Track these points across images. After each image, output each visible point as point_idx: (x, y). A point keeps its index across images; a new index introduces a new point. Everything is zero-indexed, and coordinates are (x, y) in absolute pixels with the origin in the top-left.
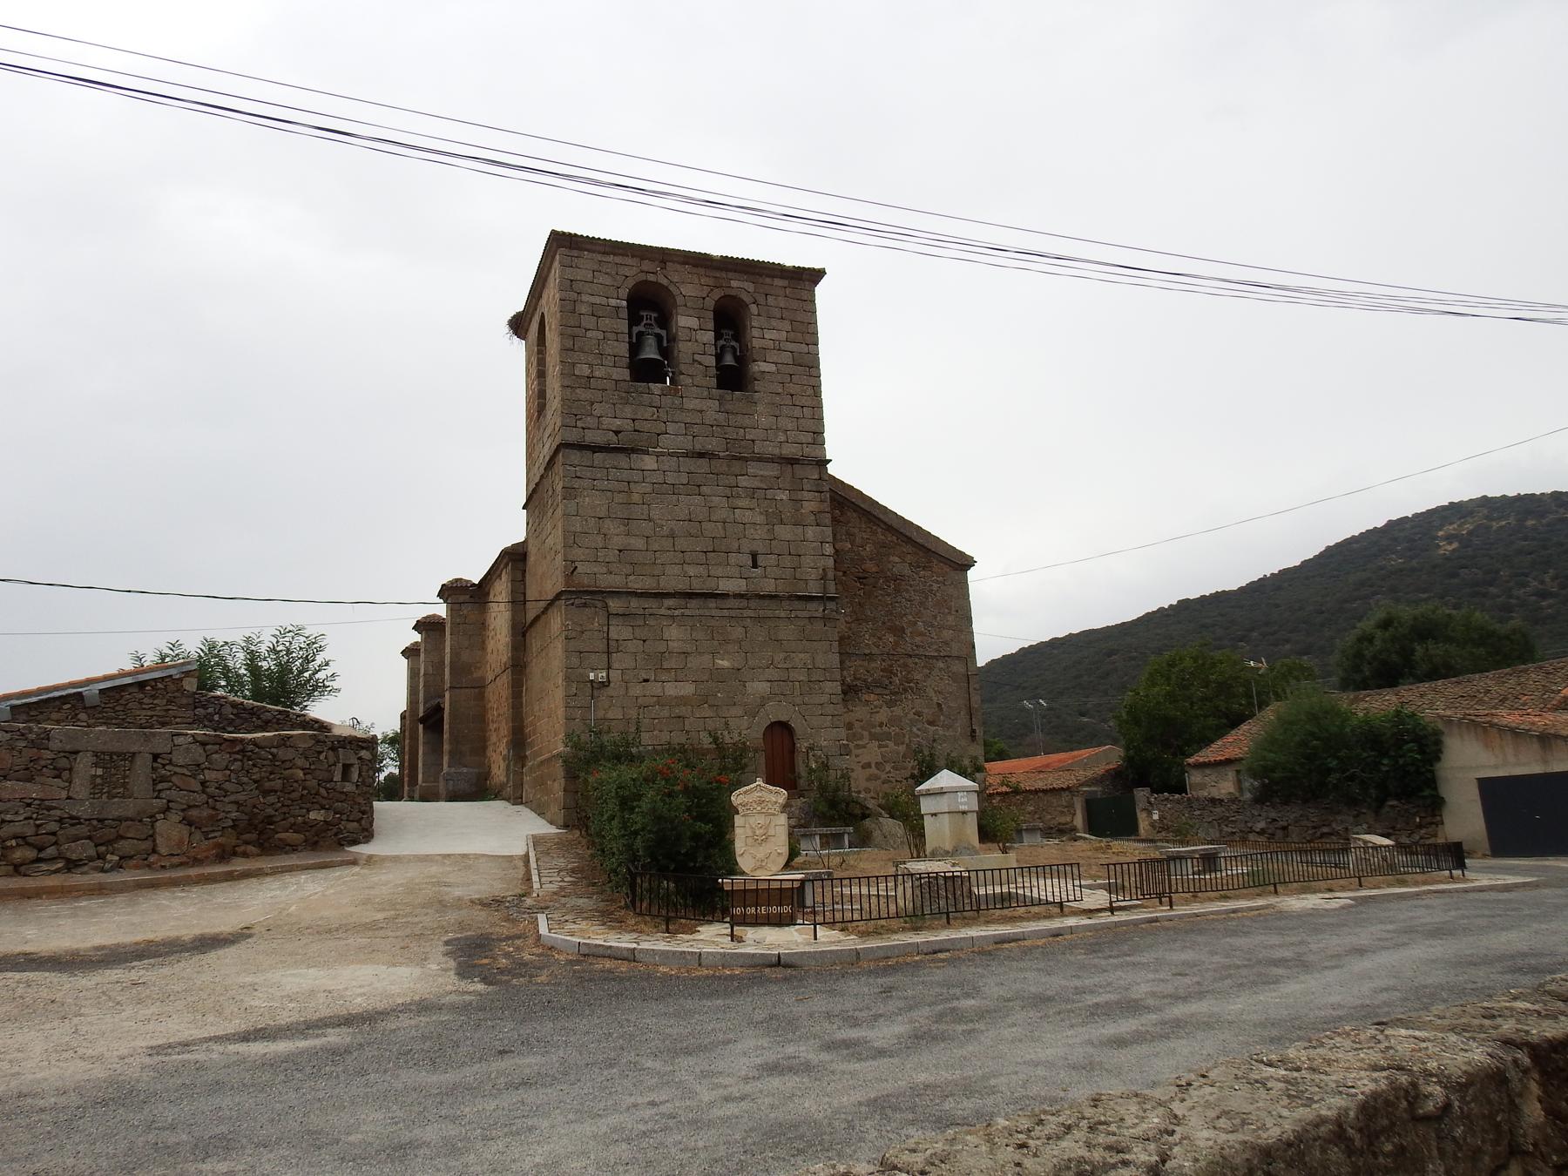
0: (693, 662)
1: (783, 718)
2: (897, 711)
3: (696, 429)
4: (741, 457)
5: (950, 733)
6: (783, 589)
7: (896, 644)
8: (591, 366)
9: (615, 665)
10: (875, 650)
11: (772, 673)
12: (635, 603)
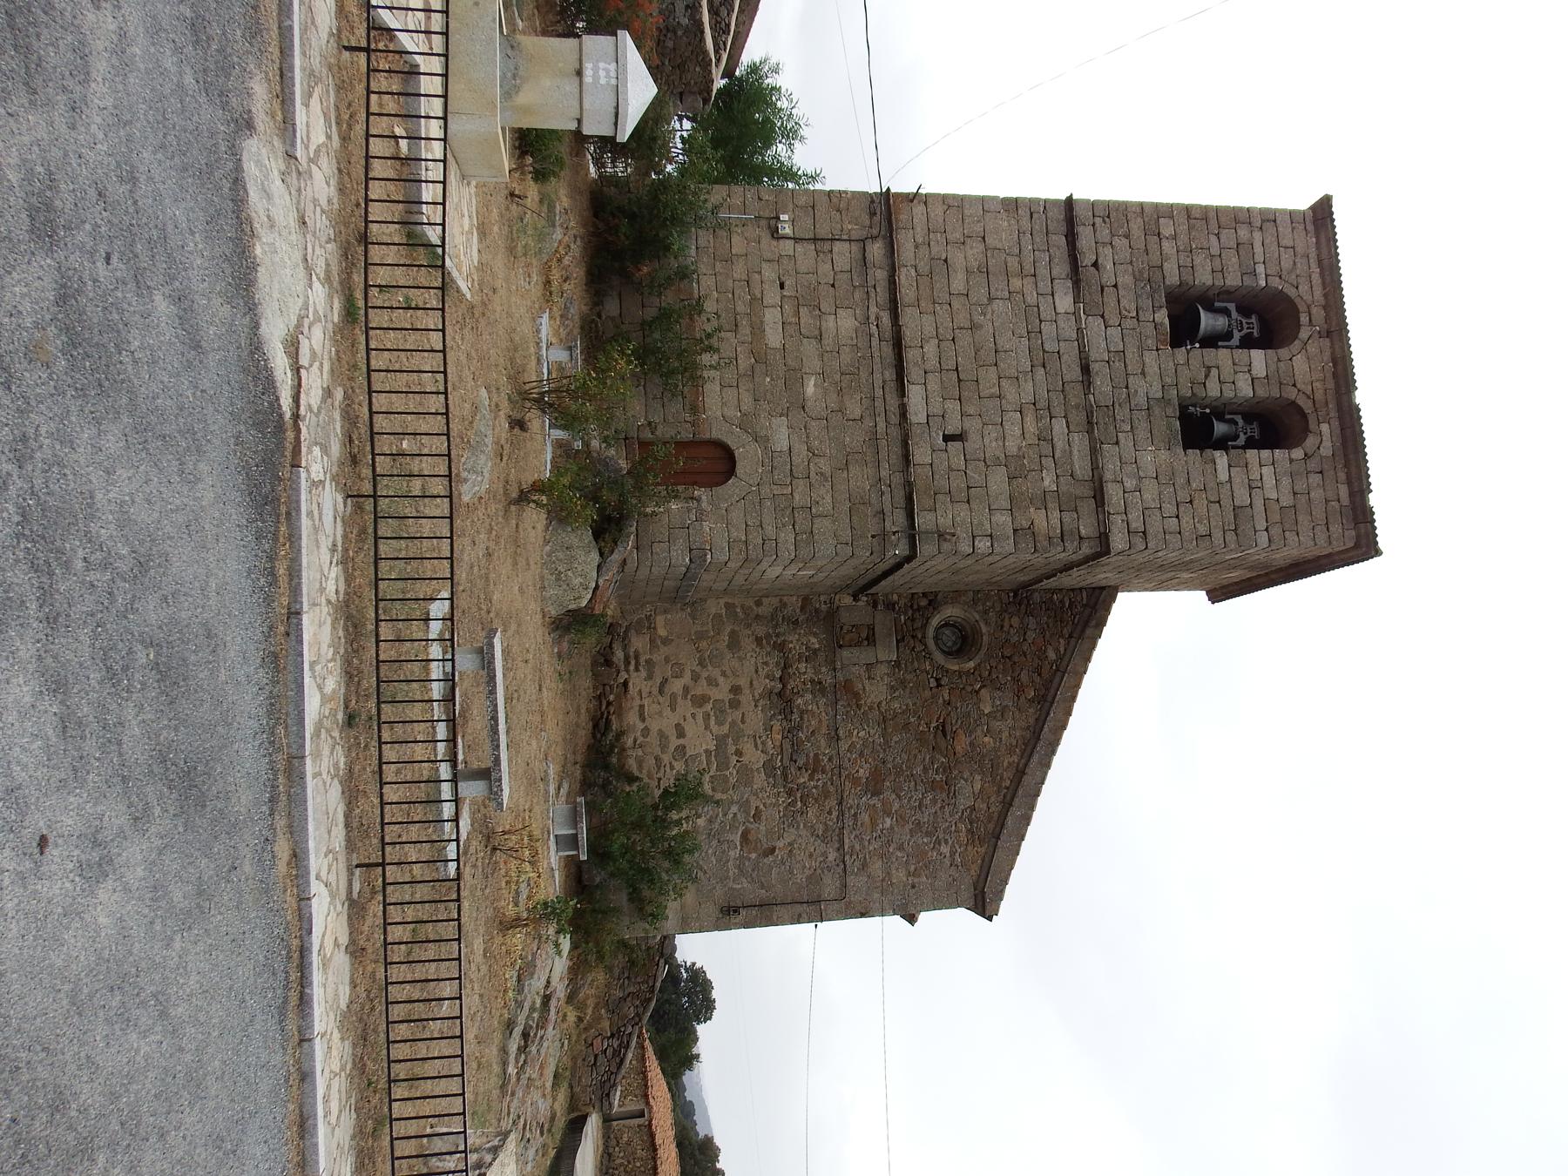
0: (809, 347)
1: (739, 470)
2: (760, 780)
3: (1118, 365)
4: (1093, 423)
6: (919, 474)
7: (856, 781)
8: (1175, 237)
9: (799, 248)
10: (844, 746)
12: (881, 275)
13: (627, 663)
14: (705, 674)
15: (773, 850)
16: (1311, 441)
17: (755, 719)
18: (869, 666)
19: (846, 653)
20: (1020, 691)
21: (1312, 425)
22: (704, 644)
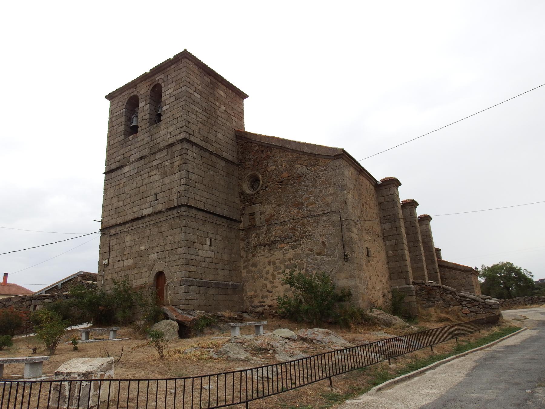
0: (134, 249)
2: (298, 250)
5: (332, 258)
7: (298, 212)
11: (158, 249)
12: (118, 229)
13: (262, 306)
14: (265, 275)
15: (323, 243)
16: (160, 82)
17: (278, 255)
18: (261, 214)
19: (257, 223)
20: (268, 157)
21: (156, 83)
22: (256, 277)
